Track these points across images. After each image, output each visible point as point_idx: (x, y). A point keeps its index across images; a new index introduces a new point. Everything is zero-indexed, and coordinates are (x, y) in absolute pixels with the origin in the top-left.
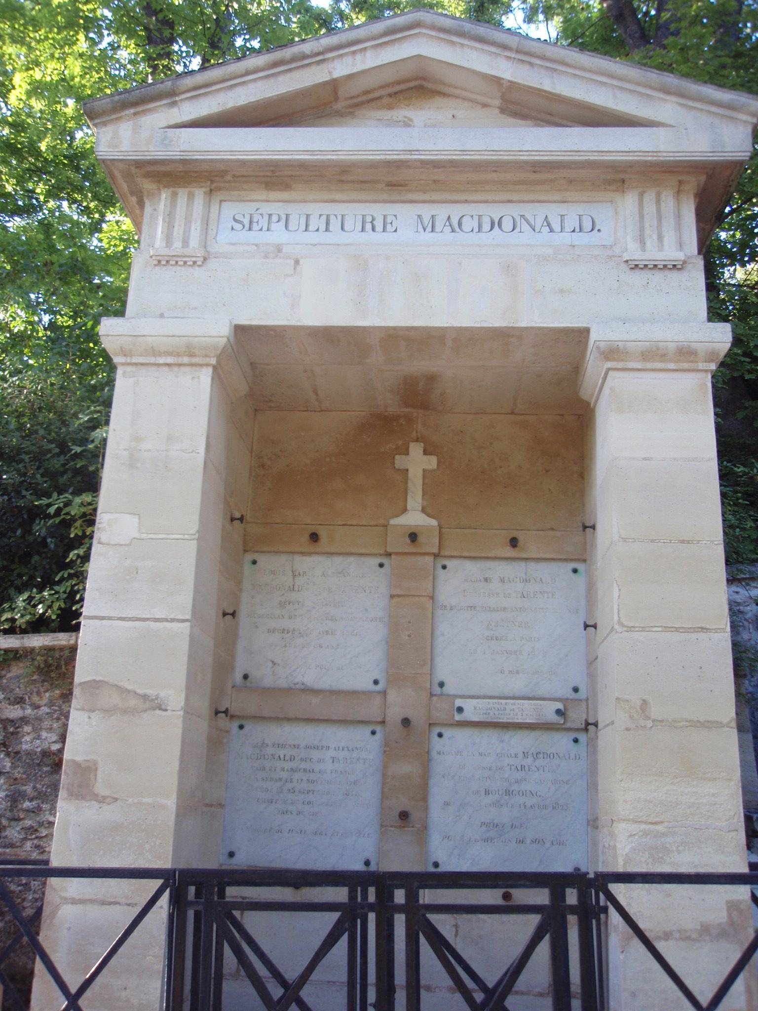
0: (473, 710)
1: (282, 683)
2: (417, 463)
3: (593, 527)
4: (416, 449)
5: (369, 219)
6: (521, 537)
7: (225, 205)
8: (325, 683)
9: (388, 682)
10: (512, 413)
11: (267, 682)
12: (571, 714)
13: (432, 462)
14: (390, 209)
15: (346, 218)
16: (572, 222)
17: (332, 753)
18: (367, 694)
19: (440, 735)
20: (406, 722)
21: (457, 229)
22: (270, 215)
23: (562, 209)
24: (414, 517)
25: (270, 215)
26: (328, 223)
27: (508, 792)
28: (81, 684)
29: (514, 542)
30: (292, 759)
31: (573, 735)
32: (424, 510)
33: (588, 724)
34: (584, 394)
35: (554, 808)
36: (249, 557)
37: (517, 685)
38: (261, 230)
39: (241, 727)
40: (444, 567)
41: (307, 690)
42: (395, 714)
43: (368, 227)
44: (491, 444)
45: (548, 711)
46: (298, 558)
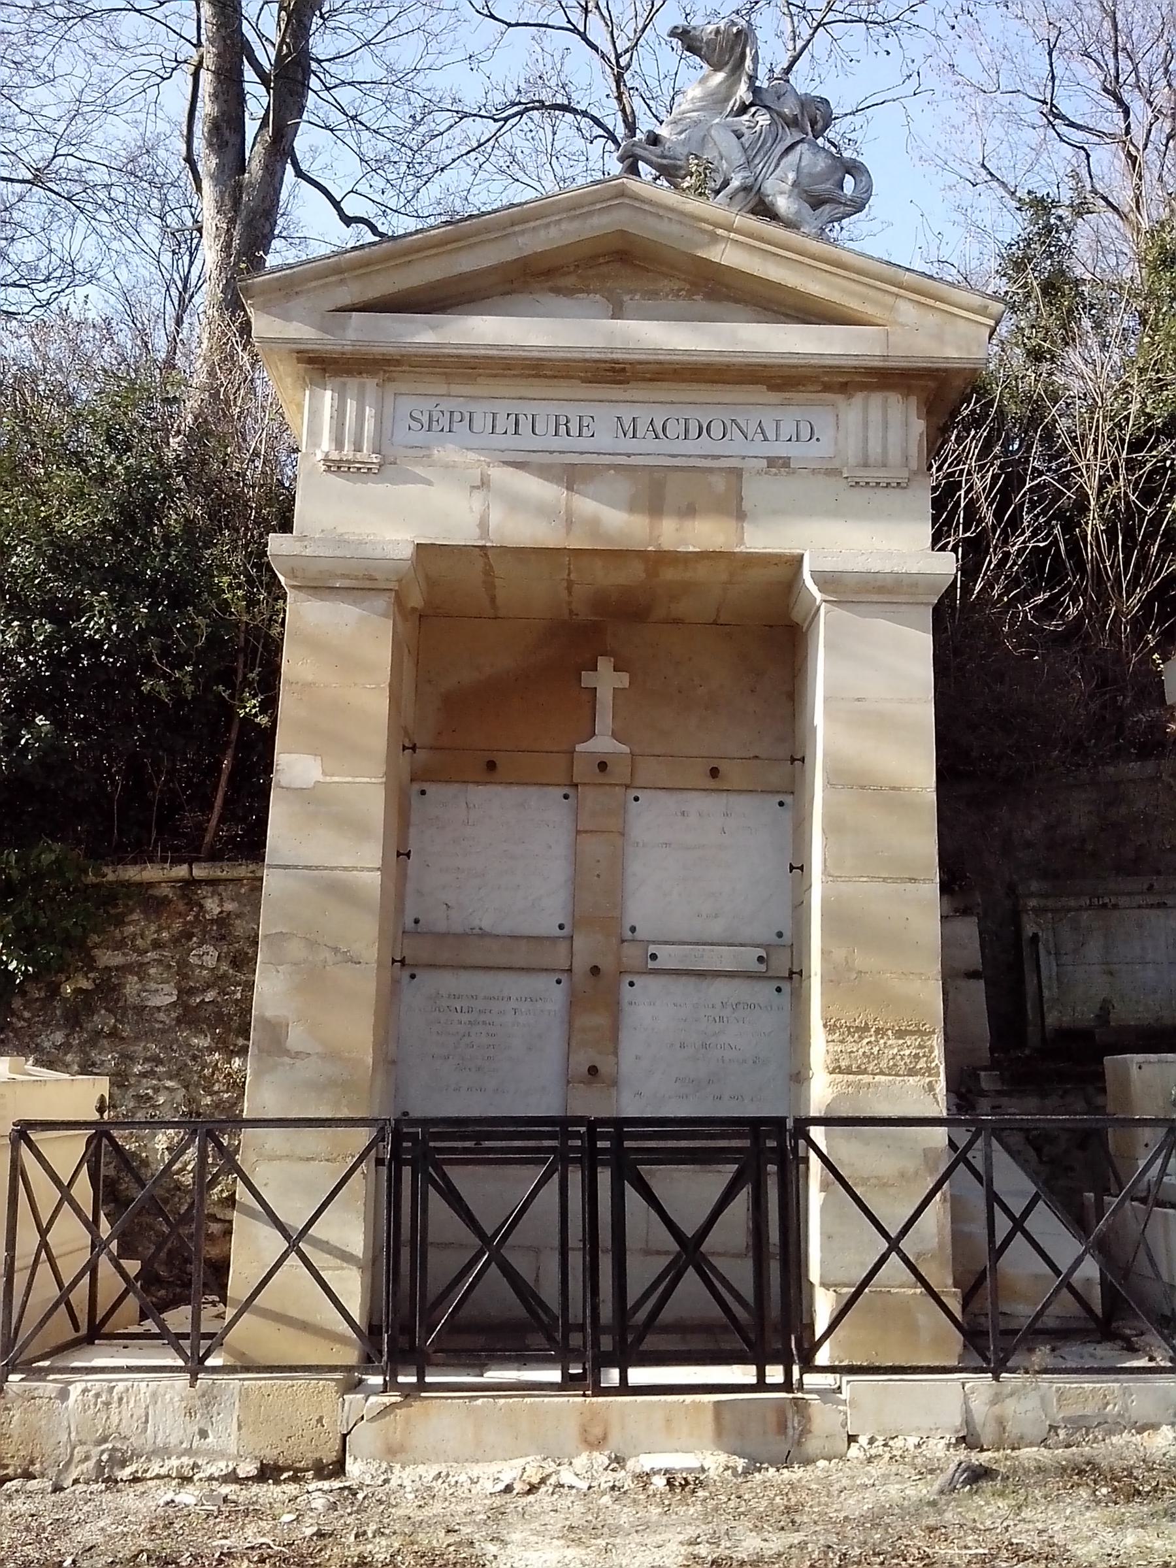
0: (668, 957)
1: (458, 928)
2: (606, 680)
3: (803, 760)
4: (605, 665)
5: (563, 420)
6: (723, 766)
7: (402, 400)
8: (505, 928)
9: (574, 926)
10: (715, 623)
11: (442, 927)
12: (774, 962)
13: (623, 680)
14: (586, 410)
15: (537, 418)
16: (788, 429)
17: (513, 1004)
18: (553, 939)
19: (632, 984)
20: (595, 970)
21: (661, 435)
22: (452, 413)
23: (778, 413)
24: (603, 743)
25: (452, 413)
26: (517, 424)
27: (705, 1046)
28: (266, 936)
29: (714, 773)
30: (470, 1010)
31: (776, 984)
32: (614, 735)
33: (791, 973)
34: (797, 615)
35: (754, 1062)
36: (416, 787)
37: (716, 929)
38: (442, 430)
39: (413, 976)
40: (636, 799)
41: (483, 935)
42: (581, 964)
43: (563, 429)
44: (690, 659)
45: (748, 958)
46: (471, 787)
